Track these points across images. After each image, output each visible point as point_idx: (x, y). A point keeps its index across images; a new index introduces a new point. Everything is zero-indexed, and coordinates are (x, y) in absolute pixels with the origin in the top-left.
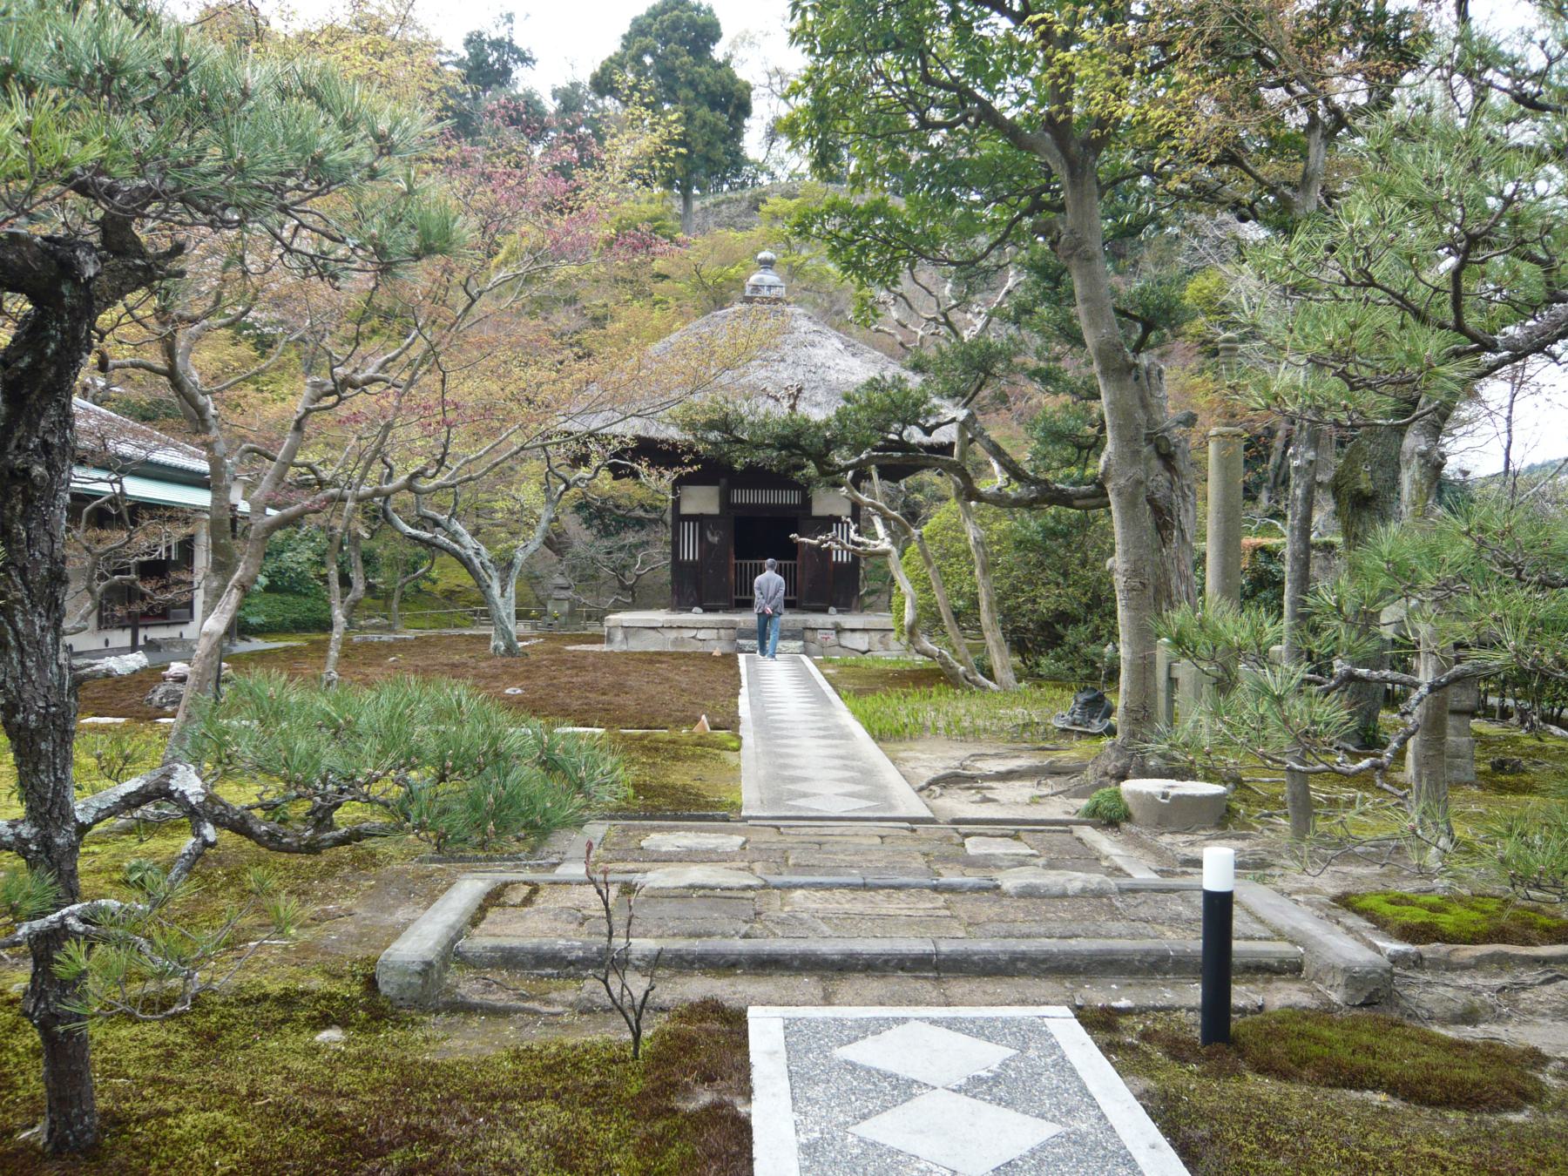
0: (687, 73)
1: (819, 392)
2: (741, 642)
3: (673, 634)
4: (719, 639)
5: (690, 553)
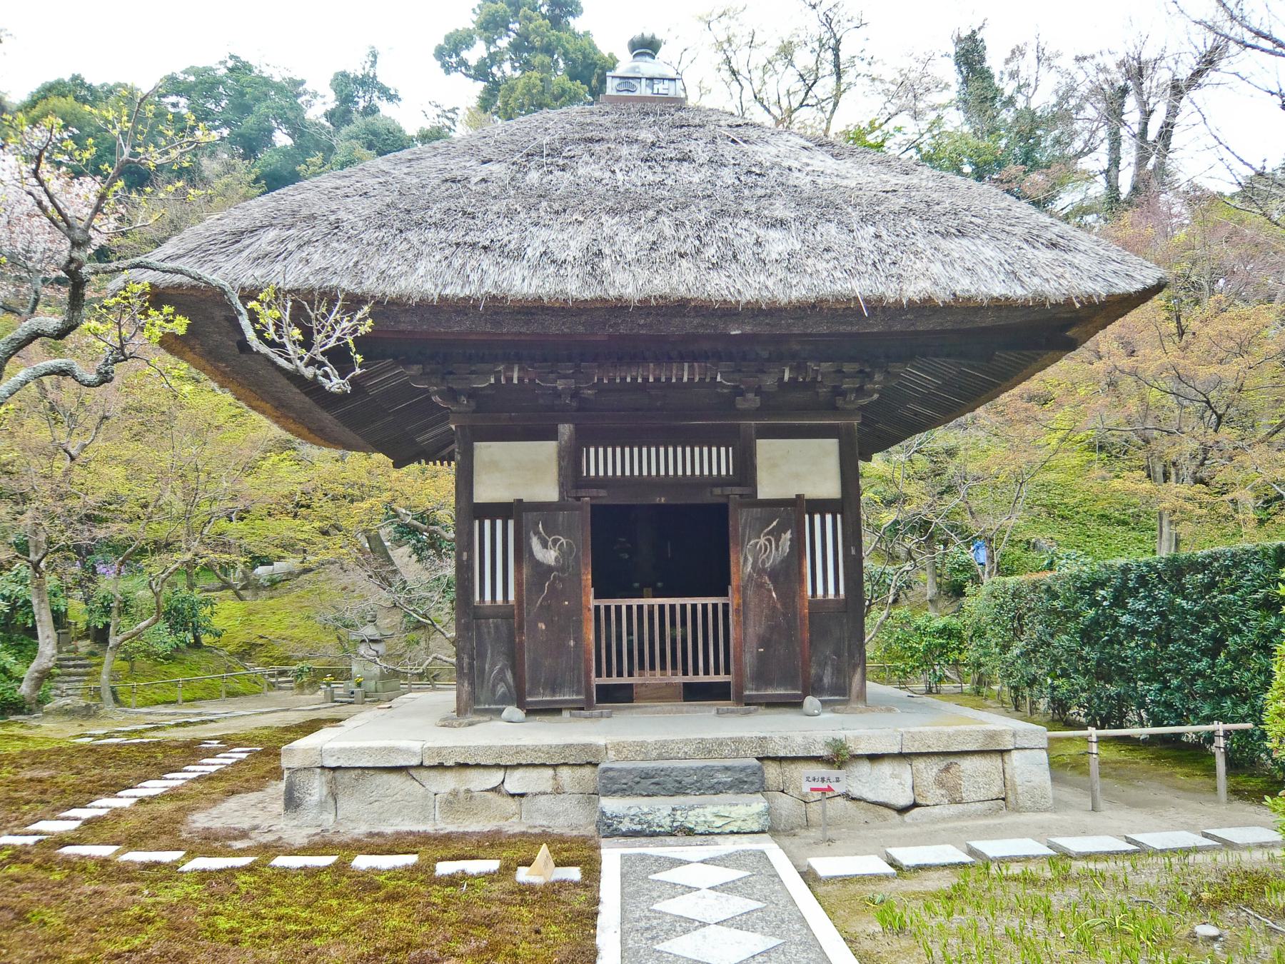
0: (542, 36)
1: (778, 203)
2: (611, 805)
3: (446, 783)
4: (558, 791)
5: (497, 588)
